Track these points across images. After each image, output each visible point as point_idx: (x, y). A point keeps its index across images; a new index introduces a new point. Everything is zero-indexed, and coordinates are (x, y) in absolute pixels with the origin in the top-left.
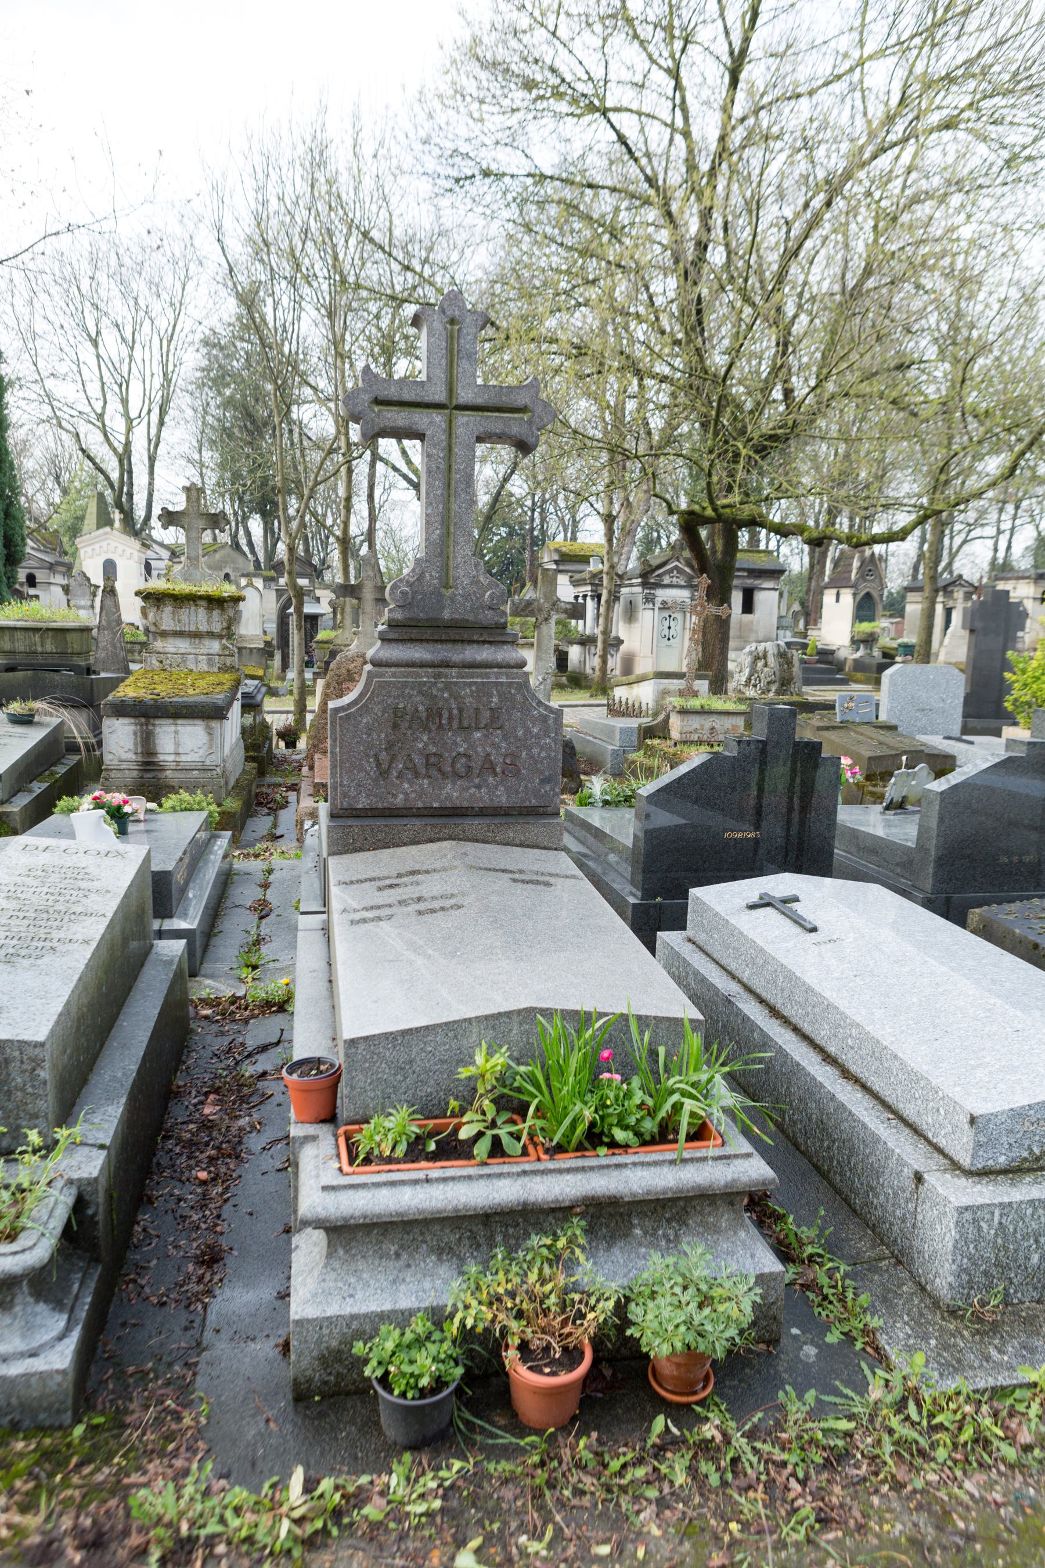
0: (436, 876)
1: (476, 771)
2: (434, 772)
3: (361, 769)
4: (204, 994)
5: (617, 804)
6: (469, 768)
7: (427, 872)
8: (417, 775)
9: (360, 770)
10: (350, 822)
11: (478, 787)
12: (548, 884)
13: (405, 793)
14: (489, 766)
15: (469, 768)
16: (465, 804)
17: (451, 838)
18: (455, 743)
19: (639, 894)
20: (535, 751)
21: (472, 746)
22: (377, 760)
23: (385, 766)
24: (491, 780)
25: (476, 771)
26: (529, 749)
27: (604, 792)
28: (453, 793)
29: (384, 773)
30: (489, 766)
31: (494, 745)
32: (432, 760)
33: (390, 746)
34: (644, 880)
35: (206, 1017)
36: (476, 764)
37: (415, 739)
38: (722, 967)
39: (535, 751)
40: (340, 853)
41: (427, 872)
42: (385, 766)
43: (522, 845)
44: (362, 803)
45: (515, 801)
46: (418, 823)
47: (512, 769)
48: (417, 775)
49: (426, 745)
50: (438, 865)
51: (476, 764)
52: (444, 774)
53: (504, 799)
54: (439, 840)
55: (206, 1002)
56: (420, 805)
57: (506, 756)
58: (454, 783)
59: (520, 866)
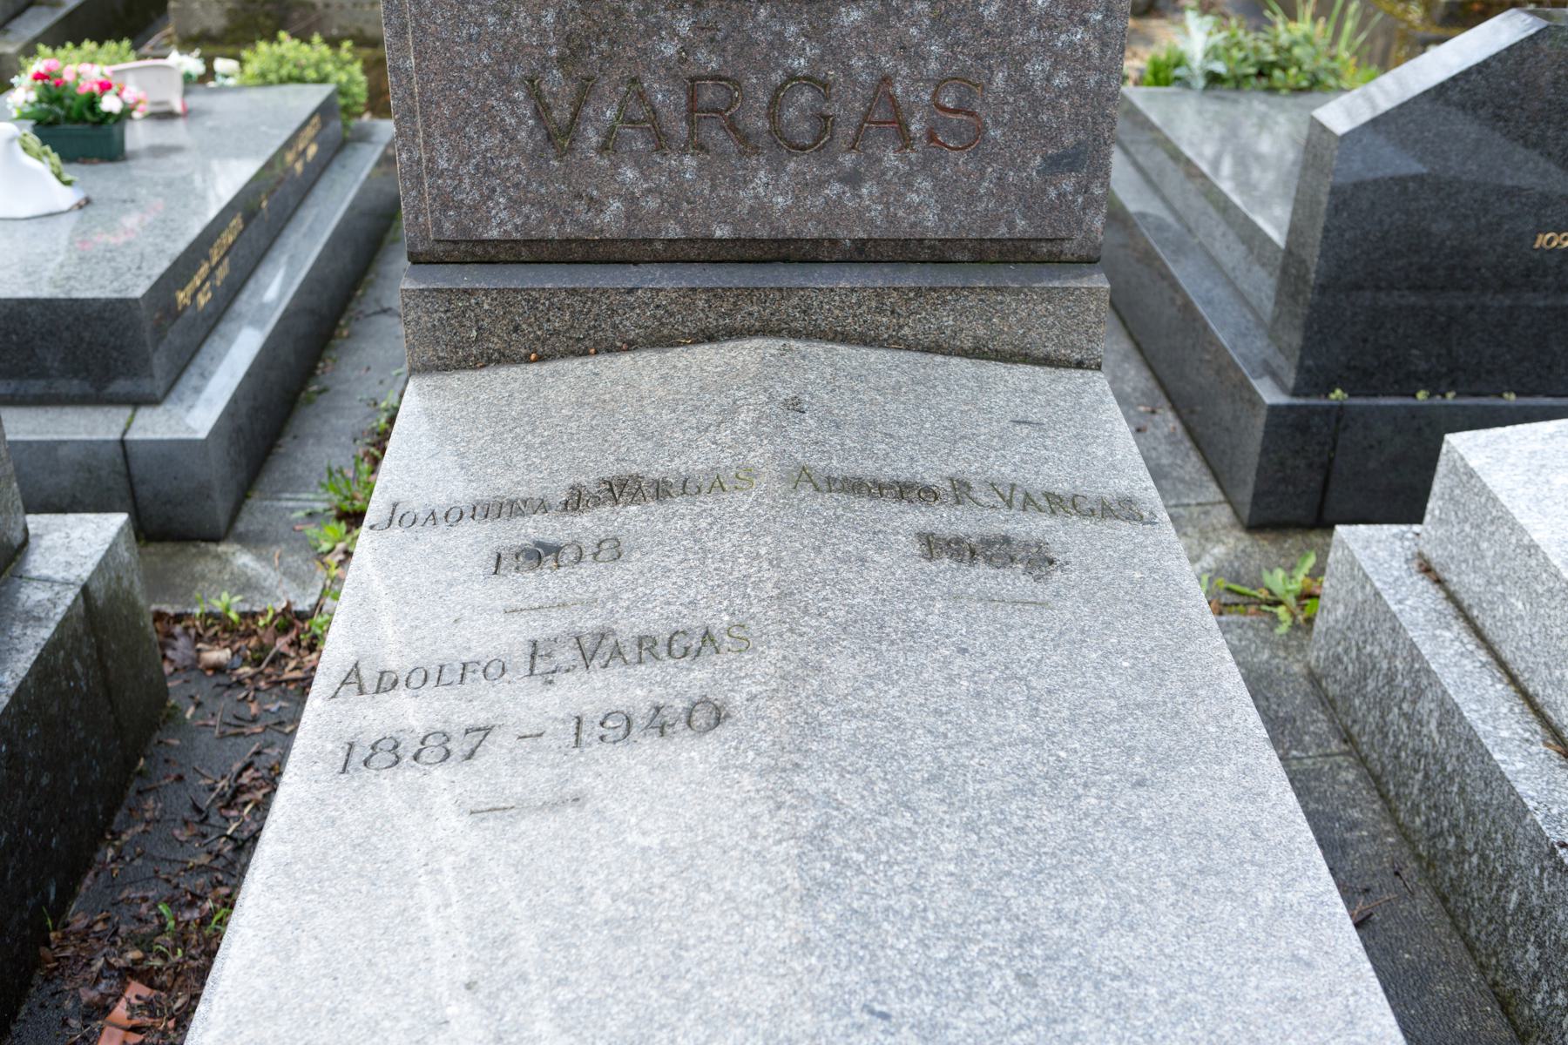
0: (682, 513)
1: (846, 132)
2: (715, 135)
3: (489, 122)
4: (227, 602)
5: (1239, 82)
6: (824, 123)
7: (661, 491)
8: (661, 141)
9: (487, 127)
10: (468, 277)
11: (853, 179)
12: (1040, 560)
13: (622, 192)
14: (887, 116)
15: (824, 123)
16: (812, 230)
17: (765, 331)
18: (780, 44)
19: (1291, 380)
20: (1036, 68)
21: (834, 52)
22: (535, 94)
23: (561, 114)
24: (891, 158)
25: (846, 132)
26: (1017, 62)
27: (1213, 53)
28: (772, 195)
29: (559, 136)
30: (887, 116)
31: (904, 49)
32: (708, 95)
33: (574, 51)
34: (1306, 350)
35: (218, 669)
36: (847, 109)
37: (654, 30)
38: (1513, 680)
39: (1036, 68)
40: (443, 367)
41: (661, 491)
42: (561, 114)
43: (978, 352)
44: (499, 224)
45: (964, 223)
46: (666, 280)
47: (960, 127)
48: (661, 141)
49: (687, 48)
50: (695, 462)
51: (847, 109)
52: (746, 142)
53: (930, 218)
54: (733, 334)
55: (221, 627)
56: (674, 230)
57: (940, 84)
58: (777, 169)
59: (964, 463)
